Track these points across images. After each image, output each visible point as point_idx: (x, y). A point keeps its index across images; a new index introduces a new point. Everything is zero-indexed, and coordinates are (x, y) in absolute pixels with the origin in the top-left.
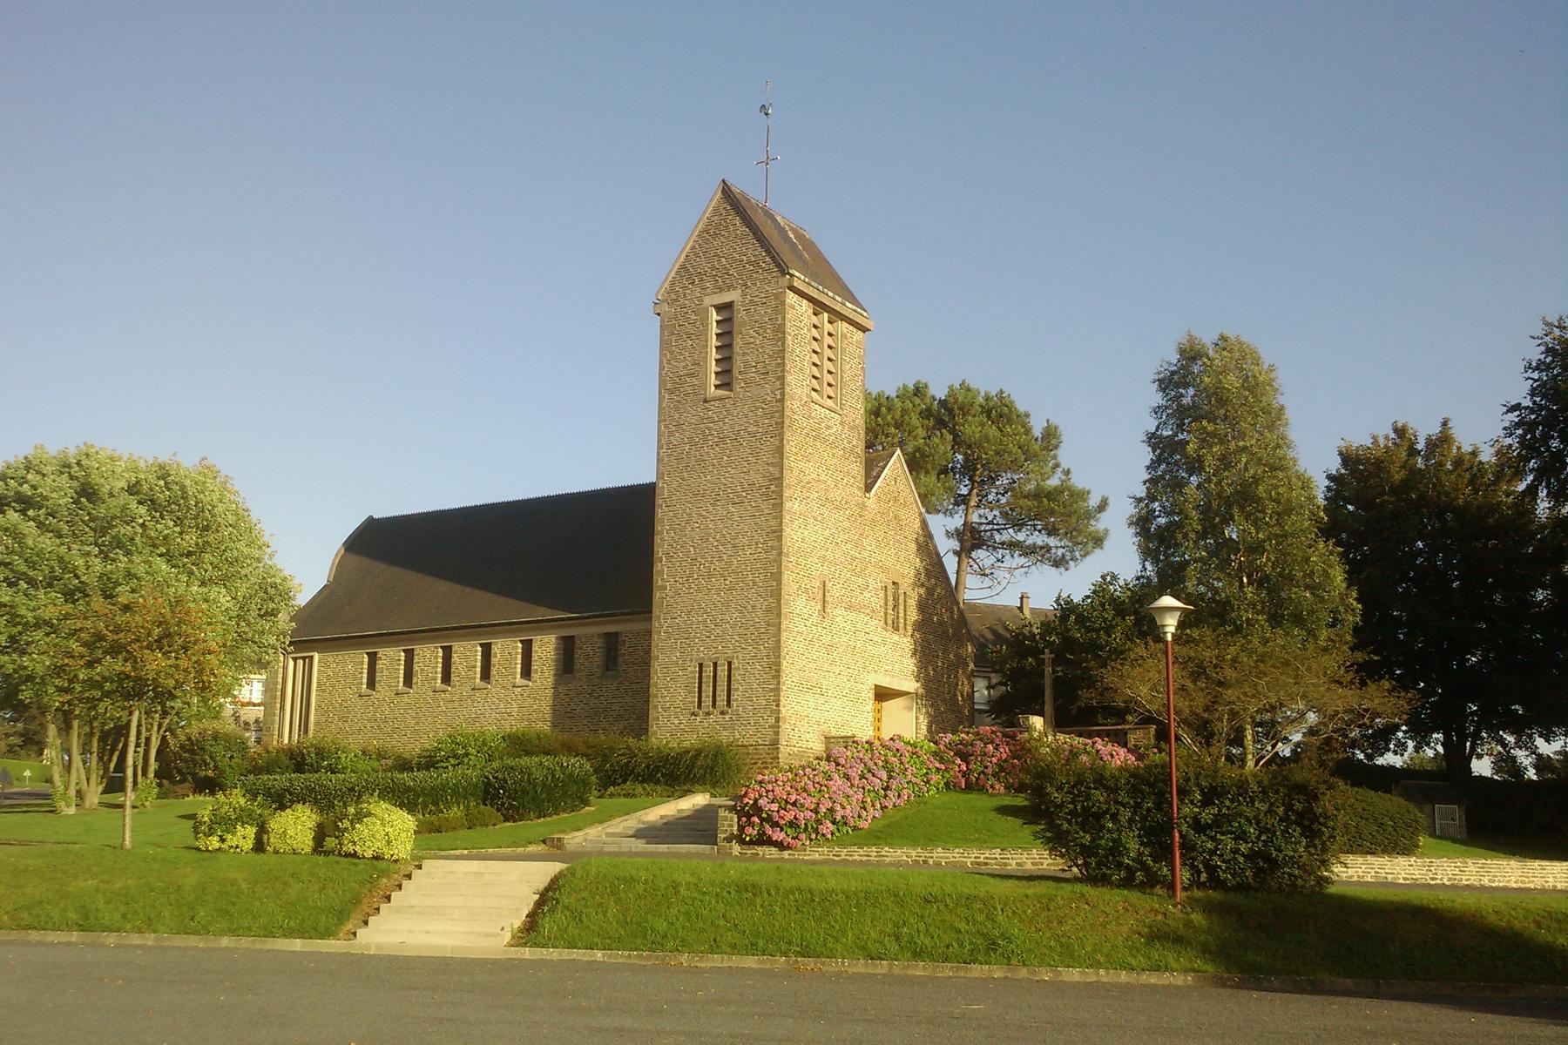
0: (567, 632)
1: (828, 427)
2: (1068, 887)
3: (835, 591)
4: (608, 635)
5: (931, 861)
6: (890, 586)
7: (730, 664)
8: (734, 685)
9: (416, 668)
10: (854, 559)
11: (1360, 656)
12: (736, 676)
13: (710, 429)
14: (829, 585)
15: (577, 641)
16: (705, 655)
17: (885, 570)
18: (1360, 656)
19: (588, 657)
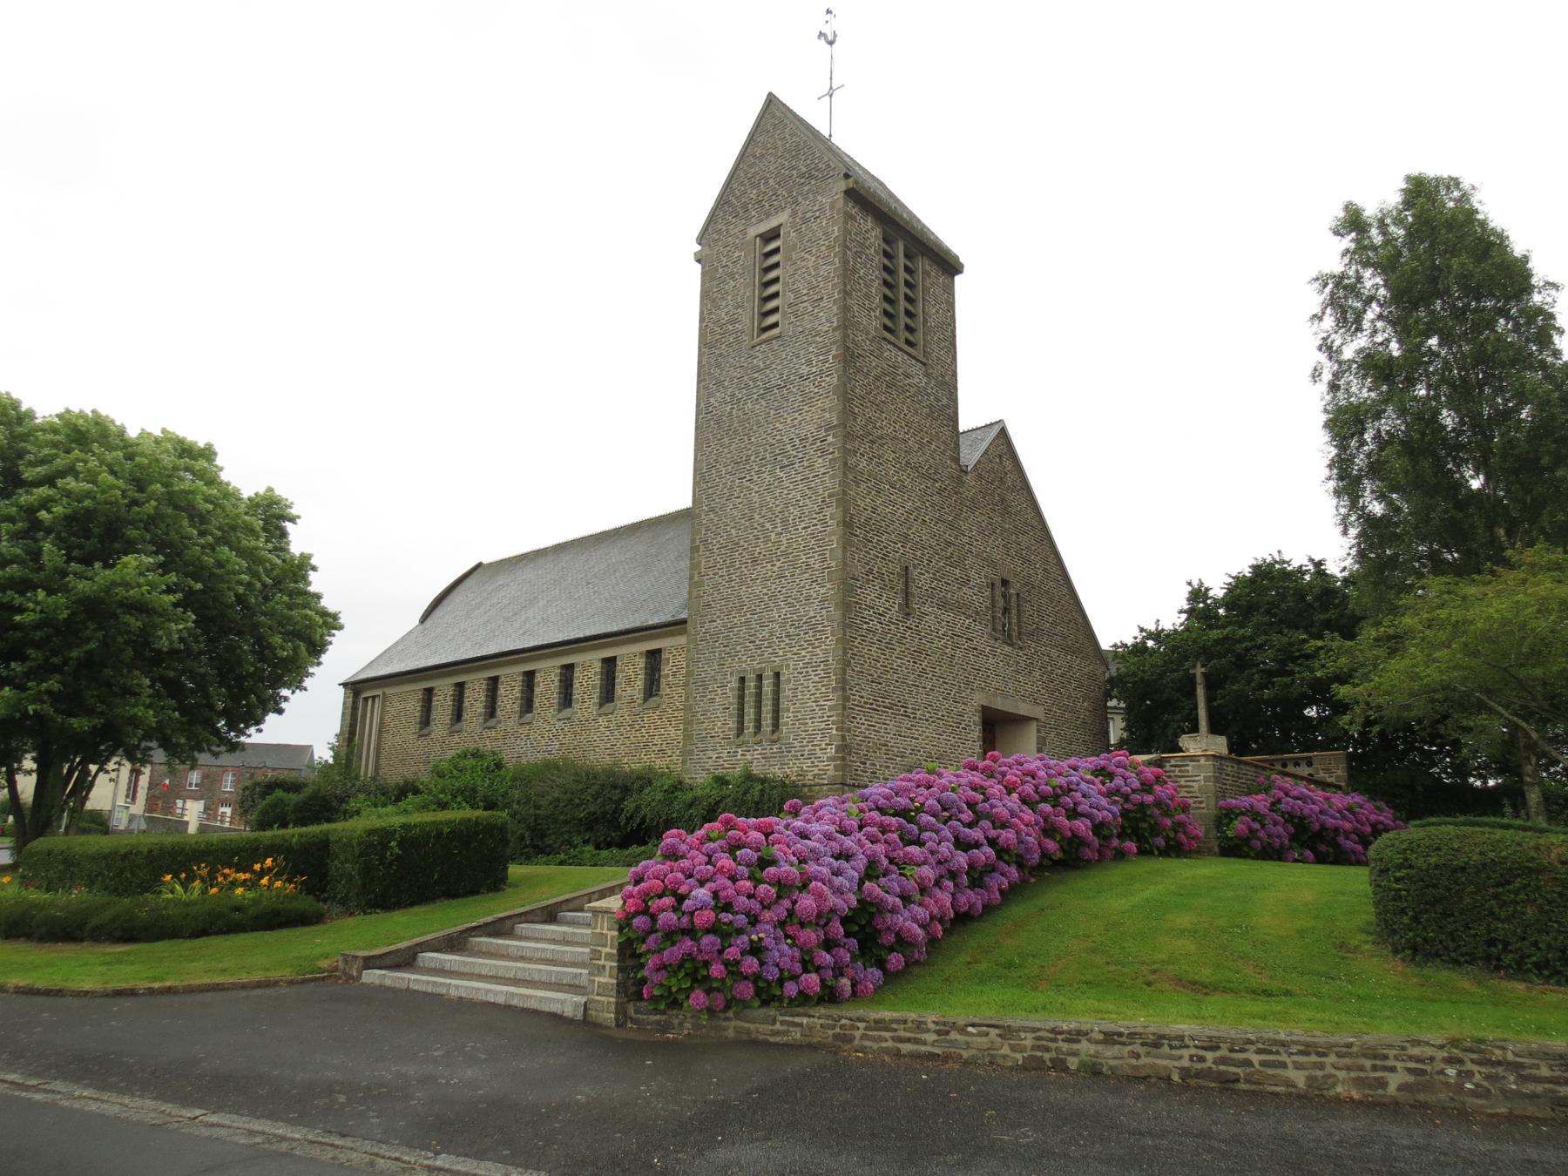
0: (608, 653)
1: (907, 376)
2: (110, 796)
3: (922, 580)
4: (649, 652)
5: (1073, 1063)
6: (998, 584)
7: (777, 675)
8: (784, 704)
9: (466, 704)
10: (949, 544)
11: (1508, 810)
12: (786, 691)
13: (754, 380)
14: (915, 573)
15: (619, 663)
16: (749, 666)
17: (993, 564)
18: (1508, 810)
19: (629, 681)
